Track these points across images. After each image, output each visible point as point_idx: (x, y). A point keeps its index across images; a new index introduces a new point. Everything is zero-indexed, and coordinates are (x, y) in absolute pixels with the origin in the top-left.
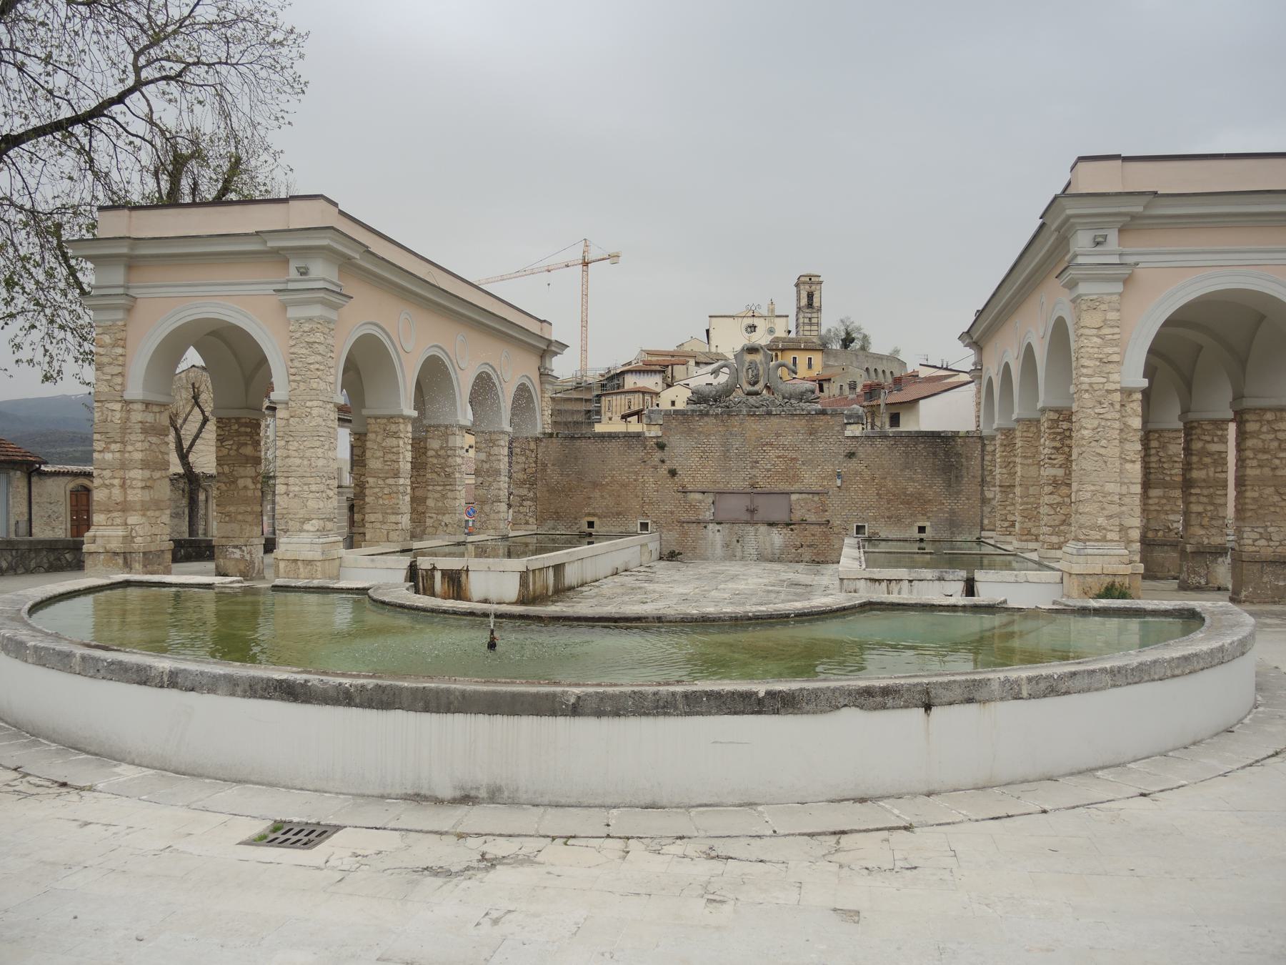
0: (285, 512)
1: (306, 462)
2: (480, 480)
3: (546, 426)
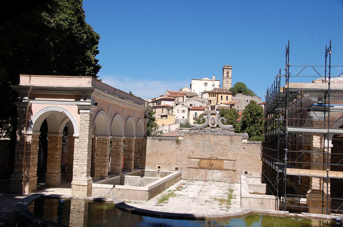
0: (76, 170)
1: (83, 156)
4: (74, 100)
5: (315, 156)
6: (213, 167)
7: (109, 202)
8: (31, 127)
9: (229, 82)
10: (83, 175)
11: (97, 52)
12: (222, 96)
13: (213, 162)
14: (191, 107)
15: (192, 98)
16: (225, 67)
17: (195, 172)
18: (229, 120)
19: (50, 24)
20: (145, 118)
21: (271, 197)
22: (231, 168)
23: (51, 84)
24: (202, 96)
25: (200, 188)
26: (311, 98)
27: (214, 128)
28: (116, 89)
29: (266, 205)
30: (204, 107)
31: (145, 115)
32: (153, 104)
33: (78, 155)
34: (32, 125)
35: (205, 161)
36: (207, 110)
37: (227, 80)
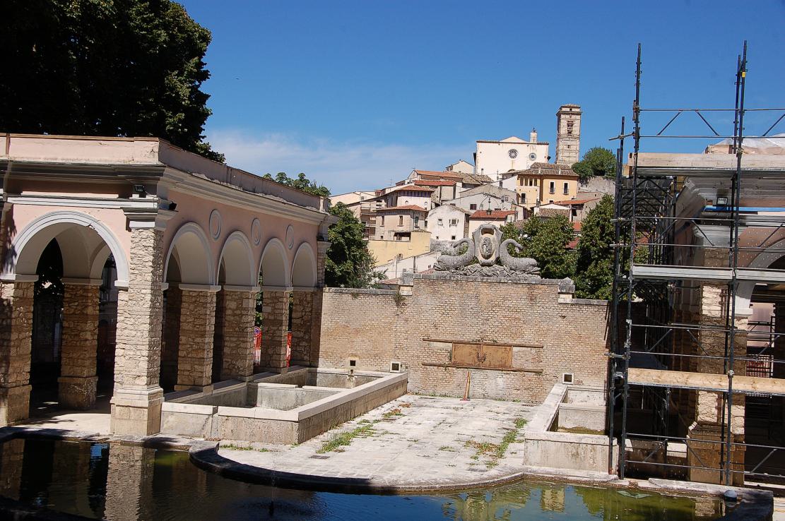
1: (139, 334)
2: (266, 328)
3: (320, 282)
4: (117, 196)
5: (708, 340)
6: (487, 362)
7: (181, 447)
8: (12, 263)
9: (573, 148)
10: (137, 381)
11: (204, 76)
12: (552, 184)
13: (485, 349)
14: (473, 212)
15: (477, 189)
16: (564, 109)
17: (440, 375)
18: (546, 244)
19: (65, 4)
20: (318, 240)
21: (599, 440)
22: (531, 367)
23: (60, 158)
24: (501, 183)
25: (444, 416)
26: (699, 192)
27: (489, 265)
28: (232, 169)
29: (584, 460)
30: (505, 210)
31: (318, 233)
32: (378, 203)
33: (126, 332)
34: (14, 257)
35: (467, 349)
36: (513, 219)
37: (569, 143)
